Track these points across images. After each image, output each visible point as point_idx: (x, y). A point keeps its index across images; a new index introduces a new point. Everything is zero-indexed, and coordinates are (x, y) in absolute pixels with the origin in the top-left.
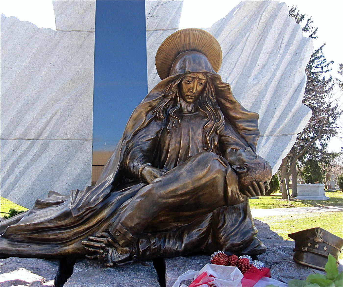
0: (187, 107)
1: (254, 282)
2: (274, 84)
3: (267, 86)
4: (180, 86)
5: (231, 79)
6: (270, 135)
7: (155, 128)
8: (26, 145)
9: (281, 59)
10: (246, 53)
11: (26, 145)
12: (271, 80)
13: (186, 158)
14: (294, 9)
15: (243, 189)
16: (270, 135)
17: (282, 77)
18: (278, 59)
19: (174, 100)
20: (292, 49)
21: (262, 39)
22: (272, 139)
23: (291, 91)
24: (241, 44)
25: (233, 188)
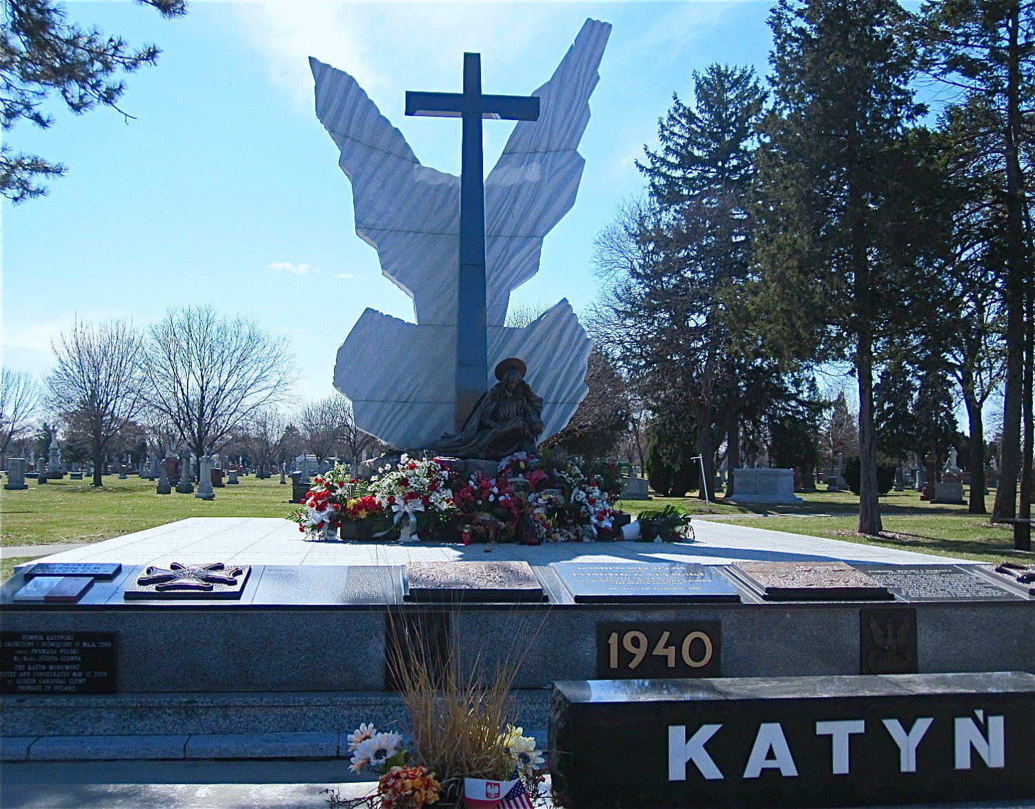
0: (509, 394)
1: (410, 152)
2: (566, 369)
3: (562, 370)
4: (506, 385)
5: (392, 710)
6: (562, 403)
7: (494, 404)
8: (398, 407)
9: (572, 352)
10: (548, 347)
11: (398, 407)
12: (564, 366)
13: (509, 419)
14: (747, 74)
15: (532, 431)
16: (562, 403)
17: (572, 365)
18: (569, 352)
19: (504, 392)
20: (579, 346)
21: (560, 337)
22: (563, 406)
23: (577, 374)
24: (545, 342)
25: (527, 431)
